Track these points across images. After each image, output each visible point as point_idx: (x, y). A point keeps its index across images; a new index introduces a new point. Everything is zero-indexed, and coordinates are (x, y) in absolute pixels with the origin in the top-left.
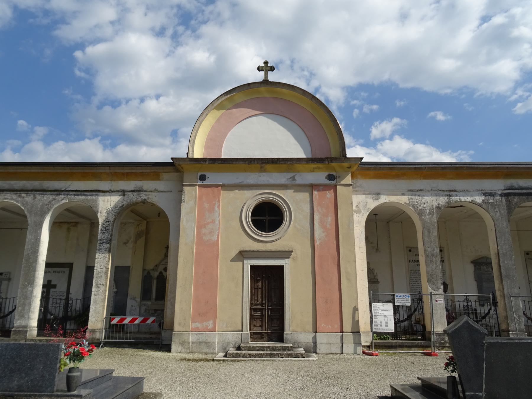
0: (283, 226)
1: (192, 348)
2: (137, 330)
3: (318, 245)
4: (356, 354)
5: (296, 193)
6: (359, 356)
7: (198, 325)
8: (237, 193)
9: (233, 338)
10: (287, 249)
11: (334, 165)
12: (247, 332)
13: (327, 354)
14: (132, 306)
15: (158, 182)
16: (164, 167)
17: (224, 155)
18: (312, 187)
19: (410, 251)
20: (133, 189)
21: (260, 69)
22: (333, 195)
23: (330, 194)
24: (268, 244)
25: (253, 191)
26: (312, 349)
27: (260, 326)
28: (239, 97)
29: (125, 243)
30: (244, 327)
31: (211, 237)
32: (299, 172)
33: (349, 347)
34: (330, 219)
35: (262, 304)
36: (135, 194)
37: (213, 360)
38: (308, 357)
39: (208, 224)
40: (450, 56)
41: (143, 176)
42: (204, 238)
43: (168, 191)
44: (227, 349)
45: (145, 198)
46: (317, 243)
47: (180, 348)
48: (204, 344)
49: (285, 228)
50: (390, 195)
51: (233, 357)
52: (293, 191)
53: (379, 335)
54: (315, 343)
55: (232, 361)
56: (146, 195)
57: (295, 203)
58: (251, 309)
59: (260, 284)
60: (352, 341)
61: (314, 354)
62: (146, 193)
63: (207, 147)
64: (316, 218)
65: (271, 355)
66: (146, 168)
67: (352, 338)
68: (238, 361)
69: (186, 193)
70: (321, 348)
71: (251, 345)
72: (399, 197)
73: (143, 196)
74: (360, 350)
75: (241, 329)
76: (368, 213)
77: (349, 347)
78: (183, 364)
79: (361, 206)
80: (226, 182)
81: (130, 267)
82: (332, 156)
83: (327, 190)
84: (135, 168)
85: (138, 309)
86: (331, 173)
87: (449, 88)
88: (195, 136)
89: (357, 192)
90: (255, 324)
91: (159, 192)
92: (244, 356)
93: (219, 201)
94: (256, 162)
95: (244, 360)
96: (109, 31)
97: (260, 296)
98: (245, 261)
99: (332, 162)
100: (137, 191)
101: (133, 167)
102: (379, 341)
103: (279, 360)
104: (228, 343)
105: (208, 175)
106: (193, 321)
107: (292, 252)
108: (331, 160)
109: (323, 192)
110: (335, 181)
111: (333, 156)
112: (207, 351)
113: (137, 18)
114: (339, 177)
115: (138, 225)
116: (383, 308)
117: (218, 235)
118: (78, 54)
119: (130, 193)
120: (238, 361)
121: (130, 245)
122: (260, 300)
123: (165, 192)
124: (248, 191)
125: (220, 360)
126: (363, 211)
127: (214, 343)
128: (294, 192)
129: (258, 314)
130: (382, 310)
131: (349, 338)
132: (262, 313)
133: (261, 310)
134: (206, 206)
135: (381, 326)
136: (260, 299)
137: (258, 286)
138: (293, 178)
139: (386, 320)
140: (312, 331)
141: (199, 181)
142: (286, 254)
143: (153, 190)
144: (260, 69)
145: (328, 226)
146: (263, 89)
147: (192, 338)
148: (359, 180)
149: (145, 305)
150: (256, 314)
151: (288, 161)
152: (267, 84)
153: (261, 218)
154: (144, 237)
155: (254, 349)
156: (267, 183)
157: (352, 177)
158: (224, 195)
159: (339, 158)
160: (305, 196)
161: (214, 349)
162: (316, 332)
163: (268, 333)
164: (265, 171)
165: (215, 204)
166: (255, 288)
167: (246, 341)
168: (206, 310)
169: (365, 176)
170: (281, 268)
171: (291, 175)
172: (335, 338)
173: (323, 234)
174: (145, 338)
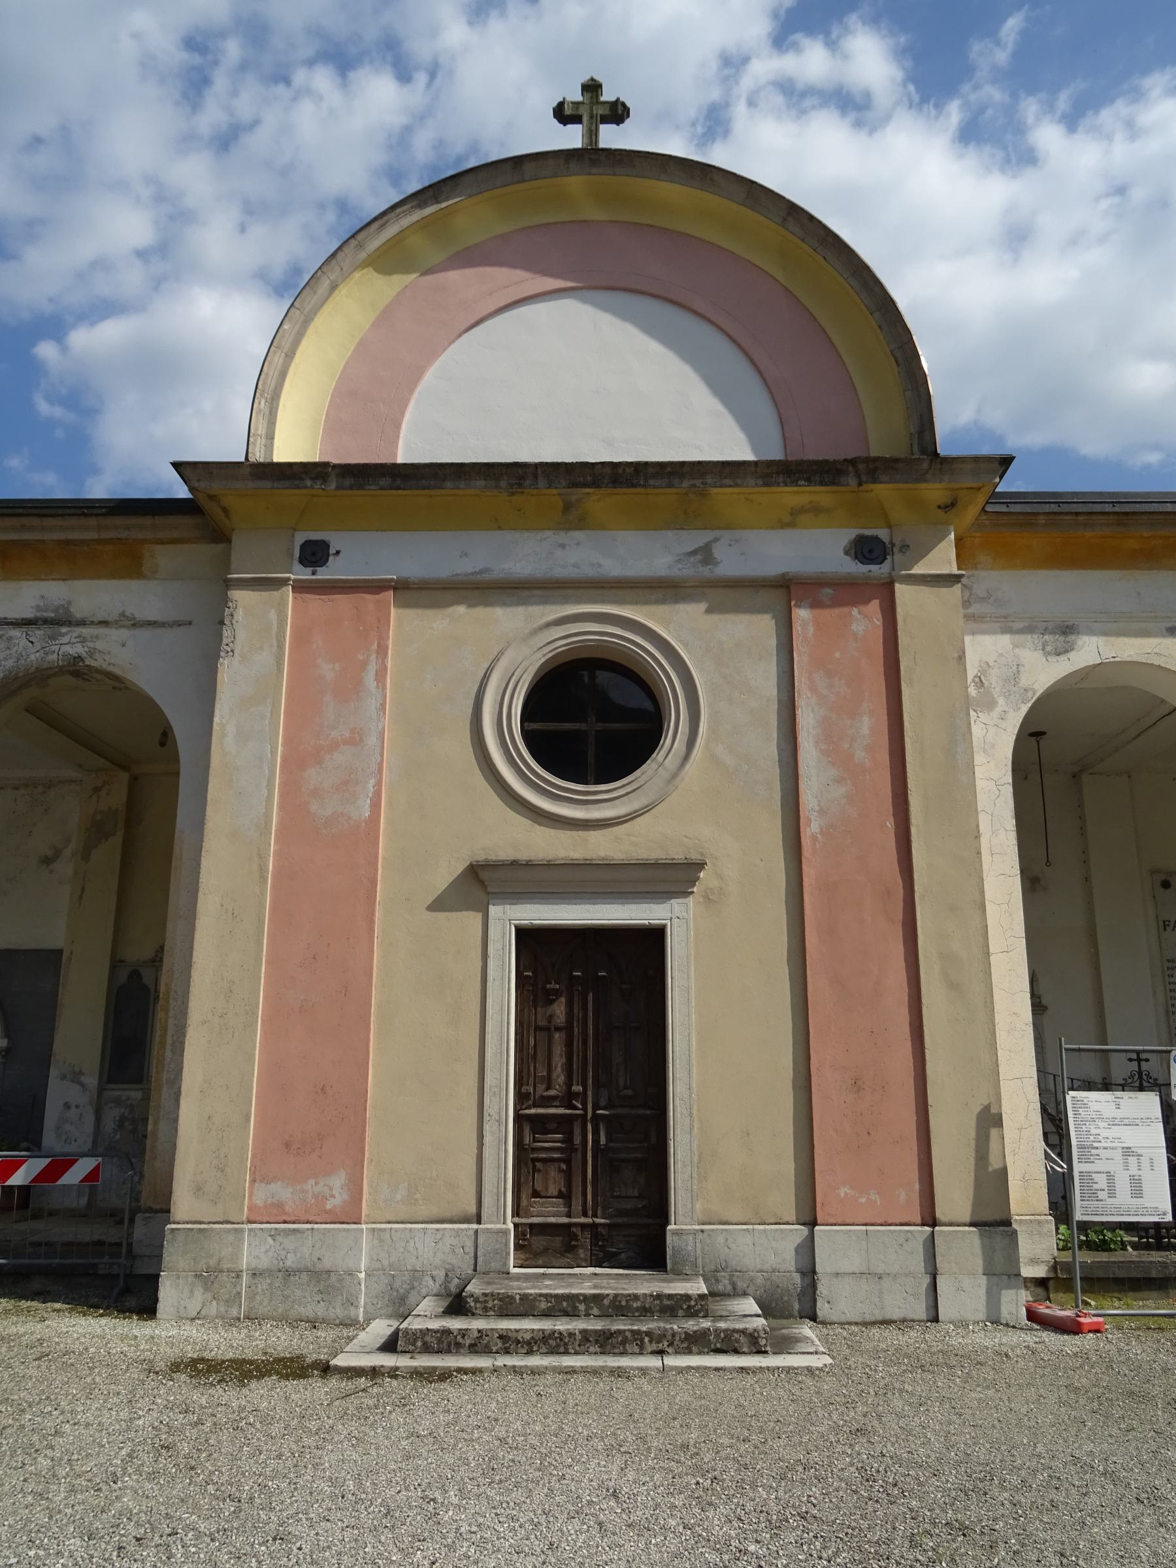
0: (659, 755)
1: (251, 1298)
2: (84, 1201)
3: (814, 838)
4: (996, 1322)
5: (715, 617)
6: (1012, 1338)
7: (282, 1192)
8: (460, 619)
9: (436, 1250)
10: (678, 855)
11: (883, 491)
12: (502, 1222)
13: (865, 1324)
14: (67, 1106)
15: (135, 584)
16: (158, 520)
17: (409, 449)
18: (786, 591)
19: (1166, 885)
20: (30, 614)
21: (568, 111)
22: (878, 621)
23: (864, 621)
24: (594, 836)
25: (531, 609)
26: (796, 1302)
27: (560, 1195)
28: (475, 218)
29: (47, 861)
30: (487, 1200)
31: (347, 808)
32: (728, 527)
33: (964, 1293)
34: (869, 726)
35: (567, 1099)
36: (38, 633)
37: (326, 1370)
38: (784, 1345)
39: (334, 746)
40: (1156, 352)
41: (73, 560)
42: (314, 808)
43: (179, 624)
44: (412, 1299)
45: (78, 649)
46: (811, 828)
47: (196, 1301)
48: (305, 1277)
49: (671, 762)
50: (1119, 634)
51: (427, 1349)
52: (703, 606)
53: (1097, 1237)
54: (809, 1272)
55: (419, 1374)
56: (83, 640)
57: (714, 659)
58: (518, 1118)
59: (559, 1010)
60: (978, 1263)
61: (806, 1330)
62: (85, 631)
63: (333, 426)
64: (806, 719)
65: (605, 1342)
66: (83, 521)
67: (978, 1250)
68: (445, 1375)
69: (240, 615)
70: (838, 1299)
71: (516, 1289)
72: (1154, 641)
73: (69, 644)
74: (1015, 1303)
75: (473, 1209)
76: (1025, 709)
77: (964, 1293)
78: (183, 1389)
79: (994, 680)
80: (413, 570)
81: (59, 953)
82: (874, 452)
83: (854, 603)
84: (35, 521)
85: (90, 1119)
86: (869, 532)
87: (1156, 447)
88: (283, 375)
89: (976, 622)
90: (539, 1187)
91: (137, 624)
92: (480, 1345)
93: (382, 651)
94: (542, 482)
95: (474, 1371)
96: (133, 279)
97: (559, 1061)
98: (494, 910)
99: (875, 480)
100: (46, 622)
101: (26, 521)
102: (1088, 1257)
103: (644, 1371)
104: (416, 1275)
105: (336, 539)
106: (260, 1176)
107: (701, 866)
108: (872, 469)
109: (837, 611)
110: (887, 565)
111: (876, 450)
112: (321, 1310)
113: (216, 238)
114: (905, 548)
115: (97, 790)
116: (1118, 1114)
117: (378, 794)
118: (46, 350)
119: (16, 633)
120: (445, 1375)
121: (65, 867)
122: (561, 1079)
123: (162, 625)
124: (510, 610)
125: (357, 1372)
126: (1001, 701)
127: (351, 1274)
128: (709, 611)
129: (552, 1142)
130: (1113, 1123)
131: (963, 1250)
132: (569, 1140)
133: (564, 1124)
134: (327, 670)
135: (1112, 1194)
136: (559, 1078)
137: (550, 1018)
138: (705, 554)
139: (1134, 1170)
140: (793, 1218)
141: (297, 566)
142: (674, 877)
143: (114, 616)
144: (568, 111)
145: (860, 754)
146: (576, 183)
147: (252, 1251)
148: (982, 573)
149: (118, 1102)
150: (543, 1139)
151: (682, 476)
152: (593, 163)
153: (567, 726)
154: (120, 834)
155: (525, 1307)
156: (589, 572)
157: (962, 557)
158: (404, 624)
159: (909, 462)
160: (757, 629)
161: (351, 1302)
162: (813, 1223)
163: (594, 1226)
164: (582, 523)
165: (364, 665)
166: (538, 1028)
167: (495, 1265)
168: (319, 1125)
169: (1011, 559)
170: (655, 937)
171: (695, 539)
172: (902, 1249)
173: (838, 791)
174: (70, 1247)
